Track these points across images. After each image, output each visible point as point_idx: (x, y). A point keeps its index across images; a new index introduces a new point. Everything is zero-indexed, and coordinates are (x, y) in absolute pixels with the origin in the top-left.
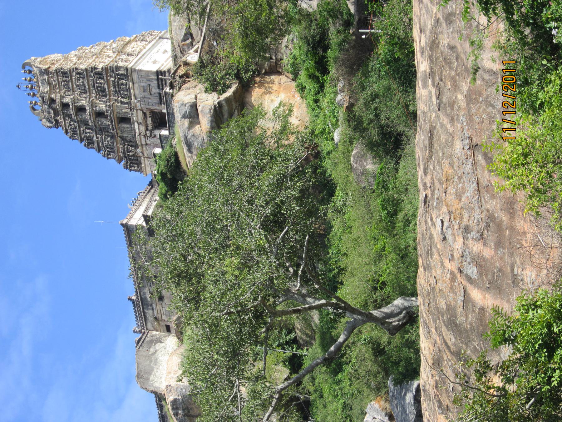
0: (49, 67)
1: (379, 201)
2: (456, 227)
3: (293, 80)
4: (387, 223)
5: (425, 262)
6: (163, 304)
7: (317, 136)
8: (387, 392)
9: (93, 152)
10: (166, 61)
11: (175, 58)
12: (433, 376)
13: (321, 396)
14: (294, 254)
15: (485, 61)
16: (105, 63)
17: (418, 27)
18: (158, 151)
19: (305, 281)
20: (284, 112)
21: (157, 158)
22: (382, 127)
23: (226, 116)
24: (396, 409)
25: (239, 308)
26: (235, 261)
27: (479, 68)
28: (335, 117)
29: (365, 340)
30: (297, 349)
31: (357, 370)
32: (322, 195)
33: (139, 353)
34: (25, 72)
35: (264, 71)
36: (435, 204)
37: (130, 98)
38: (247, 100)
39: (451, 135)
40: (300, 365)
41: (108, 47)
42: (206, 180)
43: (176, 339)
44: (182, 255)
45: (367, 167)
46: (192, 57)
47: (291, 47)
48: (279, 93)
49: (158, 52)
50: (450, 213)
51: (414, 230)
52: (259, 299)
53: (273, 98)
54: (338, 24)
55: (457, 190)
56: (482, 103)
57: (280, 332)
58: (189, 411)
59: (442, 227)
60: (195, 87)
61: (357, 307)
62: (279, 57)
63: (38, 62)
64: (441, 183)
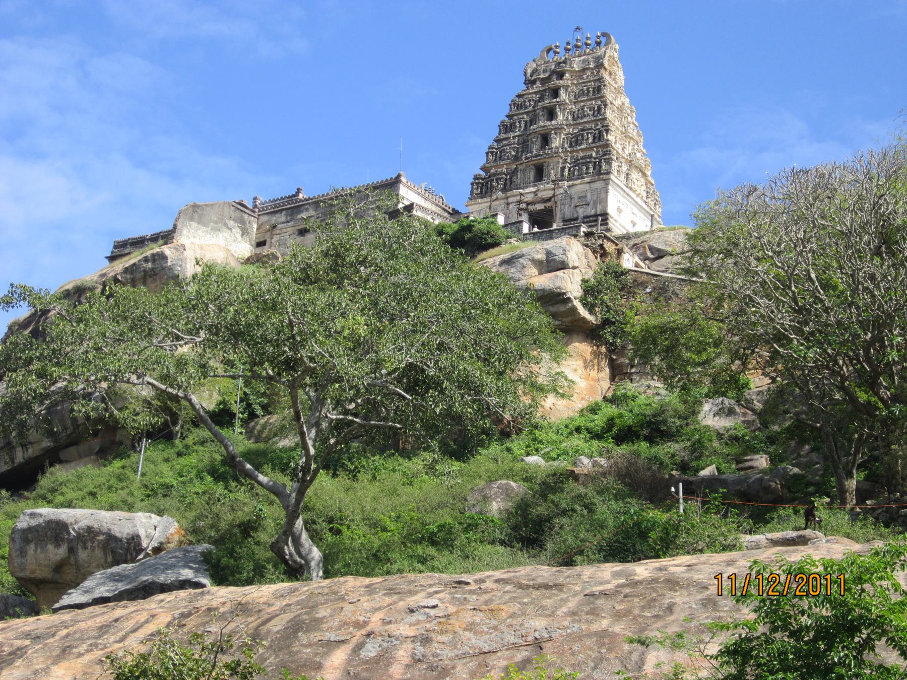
0: (606, 69)
1: (450, 521)
2: (428, 625)
3: (604, 397)
4: (420, 532)
5: (377, 586)
6: (294, 236)
7: (531, 433)
8: (191, 543)
9: (495, 133)
10: (620, 225)
11: (626, 237)
12: (224, 603)
13: (179, 454)
14: (371, 408)
15: (655, 653)
16: (615, 143)
17: (694, 561)
18: (501, 220)
19: (338, 426)
20: (561, 387)
21: (491, 219)
22: (549, 520)
23: (551, 309)
24: (170, 556)
25: (298, 338)
26: (362, 331)
27: (648, 646)
28: (559, 455)
29: (261, 510)
30: (242, 420)
31: (219, 501)
32: (452, 443)
33: (227, 205)
34: (598, 37)
35: (614, 357)
36: (458, 596)
37: (570, 179)
38: (575, 336)
39: (553, 612)
40: (221, 424)
41: (636, 147)
42: (468, 286)
44: (366, 258)
45: (494, 503)
46: (628, 260)
47: (650, 392)
48: (587, 379)
49: (633, 213)
50: (447, 616)
51: (414, 570)
52: (312, 365)
53: (580, 371)
54: (683, 454)
55: (478, 625)
56: (599, 652)
57: (264, 395)
58: (151, 277)
59: (428, 607)
60: (589, 266)
62: (634, 377)
63: (612, 53)
64: (486, 603)
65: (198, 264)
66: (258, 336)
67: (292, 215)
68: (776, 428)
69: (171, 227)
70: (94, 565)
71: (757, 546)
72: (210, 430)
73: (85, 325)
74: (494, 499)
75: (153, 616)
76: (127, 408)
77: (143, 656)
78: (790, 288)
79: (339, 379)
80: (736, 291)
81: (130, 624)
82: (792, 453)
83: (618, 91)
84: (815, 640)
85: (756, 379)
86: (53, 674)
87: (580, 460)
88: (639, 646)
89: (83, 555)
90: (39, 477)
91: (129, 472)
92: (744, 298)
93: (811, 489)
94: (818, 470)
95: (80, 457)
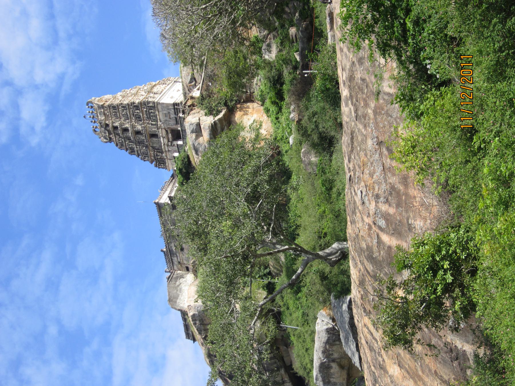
1: (320, 181)
2: (370, 195)
8: (330, 304)
9: (134, 157)
11: (185, 94)
12: (359, 291)
13: (288, 308)
14: (266, 218)
15: (384, 88)
17: (341, 67)
18: (176, 154)
19: (275, 234)
21: (176, 159)
22: (320, 133)
23: (219, 131)
25: (233, 253)
26: (229, 223)
28: (289, 128)
32: (283, 179)
34: (89, 107)
38: (232, 119)
39: (365, 136)
43: (193, 275)
44: (194, 220)
47: (259, 84)
50: (366, 186)
51: (344, 199)
57: (260, 268)
61: (309, 250)
62: (252, 91)
63: (97, 101)
64: (360, 167)
65: (197, 301)
66: (230, 274)
67: (173, 254)
68: (277, 24)
69: (179, 312)
70: (340, 350)
71: (334, 36)
72: (276, 295)
73: (226, 355)
74: (310, 159)
75: (365, 325)
76: (266, 333)
77: (384, 332)
78: (209, 18)
79: (253, 234)
80: (211, 43)
81: (369, 337)
82: (289, 16)
83: (115, 98)
84: (378, 12)
85: (253, 33)
86: (393, 374)
87: (292, 118)
88: (380, 97)
89: (336, 356)
90: (298, 375)
91: (296, 333)
92: (215, 40)
93: (306, 7)
94: (297, 4)
95: (289, 355)
